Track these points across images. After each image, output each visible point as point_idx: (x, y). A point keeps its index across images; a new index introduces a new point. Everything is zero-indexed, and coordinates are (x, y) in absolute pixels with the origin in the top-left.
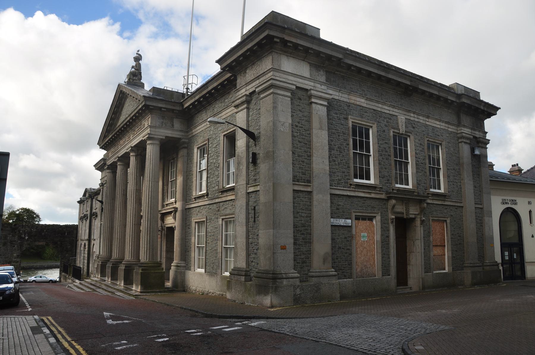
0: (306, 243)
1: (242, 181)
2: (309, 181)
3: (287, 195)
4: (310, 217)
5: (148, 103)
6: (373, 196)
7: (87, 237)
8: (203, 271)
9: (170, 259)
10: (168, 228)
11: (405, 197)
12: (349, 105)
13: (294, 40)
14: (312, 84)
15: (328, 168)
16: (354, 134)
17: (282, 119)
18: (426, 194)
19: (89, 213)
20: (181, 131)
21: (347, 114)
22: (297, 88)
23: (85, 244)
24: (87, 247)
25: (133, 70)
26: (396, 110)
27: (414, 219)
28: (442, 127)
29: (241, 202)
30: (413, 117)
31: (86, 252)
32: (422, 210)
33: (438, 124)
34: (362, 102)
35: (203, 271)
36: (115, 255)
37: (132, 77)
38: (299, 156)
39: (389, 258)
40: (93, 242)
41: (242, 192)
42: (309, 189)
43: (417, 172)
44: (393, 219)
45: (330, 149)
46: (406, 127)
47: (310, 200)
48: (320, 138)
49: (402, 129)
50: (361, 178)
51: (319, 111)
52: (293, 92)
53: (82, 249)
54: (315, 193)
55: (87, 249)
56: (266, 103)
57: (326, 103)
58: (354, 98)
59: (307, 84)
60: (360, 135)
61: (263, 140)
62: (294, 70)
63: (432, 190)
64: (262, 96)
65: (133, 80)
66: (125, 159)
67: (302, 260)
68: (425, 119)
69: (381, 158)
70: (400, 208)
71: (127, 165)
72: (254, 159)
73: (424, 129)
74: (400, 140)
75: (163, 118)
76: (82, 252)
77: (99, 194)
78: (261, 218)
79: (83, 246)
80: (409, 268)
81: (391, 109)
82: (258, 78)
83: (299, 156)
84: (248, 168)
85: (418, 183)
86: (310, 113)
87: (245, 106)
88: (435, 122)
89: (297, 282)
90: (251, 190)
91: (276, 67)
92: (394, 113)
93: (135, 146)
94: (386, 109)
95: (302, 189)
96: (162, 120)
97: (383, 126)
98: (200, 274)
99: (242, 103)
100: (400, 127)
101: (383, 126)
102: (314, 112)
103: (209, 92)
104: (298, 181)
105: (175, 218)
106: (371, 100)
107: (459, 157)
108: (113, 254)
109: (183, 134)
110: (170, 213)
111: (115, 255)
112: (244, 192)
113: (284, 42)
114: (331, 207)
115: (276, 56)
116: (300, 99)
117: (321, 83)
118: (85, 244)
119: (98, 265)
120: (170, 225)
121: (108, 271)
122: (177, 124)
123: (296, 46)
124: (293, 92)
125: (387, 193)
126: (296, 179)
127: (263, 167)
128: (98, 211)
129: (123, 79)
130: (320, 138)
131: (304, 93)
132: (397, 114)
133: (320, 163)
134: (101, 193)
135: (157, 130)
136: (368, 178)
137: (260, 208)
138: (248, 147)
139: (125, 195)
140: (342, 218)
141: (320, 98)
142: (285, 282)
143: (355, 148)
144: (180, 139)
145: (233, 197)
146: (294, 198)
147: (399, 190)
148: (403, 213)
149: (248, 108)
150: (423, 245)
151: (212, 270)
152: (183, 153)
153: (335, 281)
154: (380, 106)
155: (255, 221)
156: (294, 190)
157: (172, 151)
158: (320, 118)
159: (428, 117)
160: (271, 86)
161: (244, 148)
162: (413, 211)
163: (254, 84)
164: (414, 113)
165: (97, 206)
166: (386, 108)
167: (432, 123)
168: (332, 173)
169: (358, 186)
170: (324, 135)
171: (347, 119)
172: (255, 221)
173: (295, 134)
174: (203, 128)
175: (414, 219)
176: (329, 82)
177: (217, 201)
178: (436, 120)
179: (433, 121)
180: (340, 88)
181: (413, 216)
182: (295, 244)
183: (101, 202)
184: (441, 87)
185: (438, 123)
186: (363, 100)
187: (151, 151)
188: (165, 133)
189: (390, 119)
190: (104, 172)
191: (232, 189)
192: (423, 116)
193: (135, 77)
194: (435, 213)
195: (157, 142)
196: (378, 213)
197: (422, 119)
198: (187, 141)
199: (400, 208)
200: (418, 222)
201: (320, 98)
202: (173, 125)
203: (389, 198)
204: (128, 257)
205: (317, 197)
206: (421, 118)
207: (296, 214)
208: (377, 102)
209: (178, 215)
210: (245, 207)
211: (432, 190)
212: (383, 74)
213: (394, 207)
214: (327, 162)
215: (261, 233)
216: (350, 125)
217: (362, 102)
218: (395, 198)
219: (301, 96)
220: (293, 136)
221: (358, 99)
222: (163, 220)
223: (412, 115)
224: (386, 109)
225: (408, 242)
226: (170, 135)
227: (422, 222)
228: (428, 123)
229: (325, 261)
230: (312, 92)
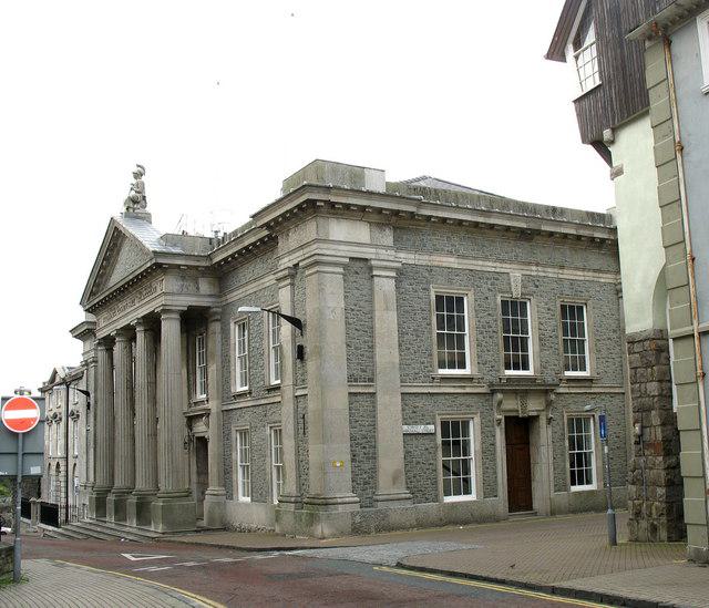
0: (368, 458)
1: (289, 381)
2: (371, 380)
3: (339, 399)
4: (374, 425)
5: (160, 261)
6: (468, 390)
7: (60, 453)
8: (249, 499)
9: (203, 485)
10: (198, 438)
11: (522, 389)
12: (430, 269)
13: (344, 200)
14: (373, 250)
15: (397, 361)
16: (438, 308)
17: (331, 304)
18: (556, 381)
19: (63, 409)
20: (210, 296)
21: (428, 283)
22: (351, 259)
23: (58, 465)
24: (62, 468)
25: (133, 193)
26: (508, 266)
27: (538, 416)
28: (587, 278)
29: (288, 409)
30: (534, 270)
31: (62, 479)
32: (549, 404)
33: (579, 275)
34: (452, 262)
35: (249, 499)
36: (120, 482)
37: (131, 205)
38: (356, 348)
39: (495, 473)
40: (71, 462)
41: (288, 393)
42: (371, 390)
43: (541, 350)
44: (500, 420)
45: (401, 333)
46: (524, 286)
47: (374, 404)
48: (386, 321)
49: (517, 292)
50: (452, 366)
51: (385, 286)
52: (345, 266)
53: (53, 472)
54: (379, 396)
55: (63, 473)
56: (310, 282)
57: (394, 274)
58: (438, 259)
59: (368, 253)
60: (450, 306)
61: (308, 330)
62: (347, 236)
63: (568, 373)
64: (307, 273)
65: (134, 209)
66: (129, 333)
67: (364, 478)
68: (556, 270)
69: (481, 337)
70: (511, 404)
71: (133, 338)
72: (300, 353)
73: (555, 285)
74: (513, 308)
75: (183, 278)
76: (53, 478)
77: (81, 378)
78: (311, 429)
79: (54, 468)
80: (534, 485)
81: (498, 264)
82: (302, 247)
83: (356, 348)
84: (295, 364)
85: (543, 367)
86: (372, 289)
87: (288, 281)
88: (575, 272)
89: (357, 508)
90: (299, 393)
91: (322, 236)
92: (502, 270)
93: (143, 317)
94: (490, 266)
95: (360, 390)
96: (180, 283)
97: (484, 290)
98: (246, 504)
99: (285, 278)
100: (513, 290)
101: (484, 290)
102: (376, 289)
103: (246, 248)
104: (356, 380)
105: (207, 425)
106: (464, 257)
107: (618, 320)
108: (116, 482)
109: (214, 300)
110: (202, 416)
111: (120, 482)
112: (291, 396)
113: (332, 205)
114: (403, 410)
115: (321, 221)
116: (357, 273)
117: (386, 247)
118: (58, 465)
119: (90, 498)
120: (202, 435)
121: (110, 506)
122: (205, 286)
123: (347, 207)
124: (345, 266)
125: (491, 385)
126: (352, 379)
127: (311, 365)
128: (82, 410)
129: (117, 209)
130: (386, 321)
131: (362, 264)
132: (508, 271)
133: (387, 353)
134: (85, 378)
135: (176, 298)
136: (462, 365)
137: (310, 417)
138: (294, 336)
139: (131, 388)
140: (422, 423)
141: (386, 268)
142: (340, 508)
143: (440, 327)
144: (209, 307)
145: (278, 399)
146: (351, 403)
147: (509, 379)
148: (517, 411)
149: (292, 284)
150: (551, 453)
151: (259, 493)
152: (215, 327)
153: (409, 505)
154: (480, 263)
155: (304, 433)
156: (350, 393)
157: (195, 322)
158: (385, 296)
159: (562, 267)
160: (317, 263)
161: (290, 338)
162: (533, 406)
163: (297, 254)
164: (537, 265)
165: (77, 399)
166: (490, 264)
167: (568, 274)
168: (403, 365)
169: (445, 379)
170: (392, 316)
171: (427, 289)
172: (304, 433)
173: (351, 321)
174: (252, 294)
175: (538, 416)
176: (399, 245)
177: (263, 402)
178: (577, 269)
179: (570, 272)
180: (418, 249)
181: (535, 414)
182: (353, 460)
183: (87, 393)
184: (83, 561)
185: (579, 273)
186: (452, 260)
187: (170, 330)
188: (185, 301)
189: (497, 279)
190: (88, 343)
191: (277, 388)
192: (553, 267)
193: (136, 203)
194: (572, 406)
195: (177, 316)
196: (476, 414)
197: (551, 272)
198: (219, 310)
199: (511, 404)
200: (543, 421)
201: (386, 268)
202: (198, 288)
203: (493, 392)
204: (141, 485)
205: (381, 399)
206: (549, 270)
207: (353, 422)
208: (475, 258)
209: (213, 419)
210: (292, 416)
211: (568, 373)
212: (481, 220)
213: (500, 403)
214: (397, 354)
215: (311, 447)
216: (433, 298)
217: (452, 262)
218: (502, 391)
219: (359, 268)
220: (347, 323)
221: (445, 259)
222: (190, 427)
223: (534, 268)
224: (490, 266)
225: (532, 450)
226: (194, 304)
227: (549, 421)
228: (561, 276)
229: (395, 479)
230: (373, 262)
